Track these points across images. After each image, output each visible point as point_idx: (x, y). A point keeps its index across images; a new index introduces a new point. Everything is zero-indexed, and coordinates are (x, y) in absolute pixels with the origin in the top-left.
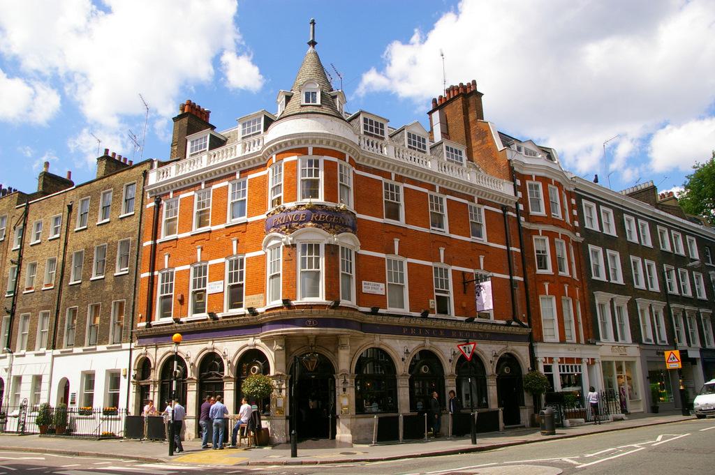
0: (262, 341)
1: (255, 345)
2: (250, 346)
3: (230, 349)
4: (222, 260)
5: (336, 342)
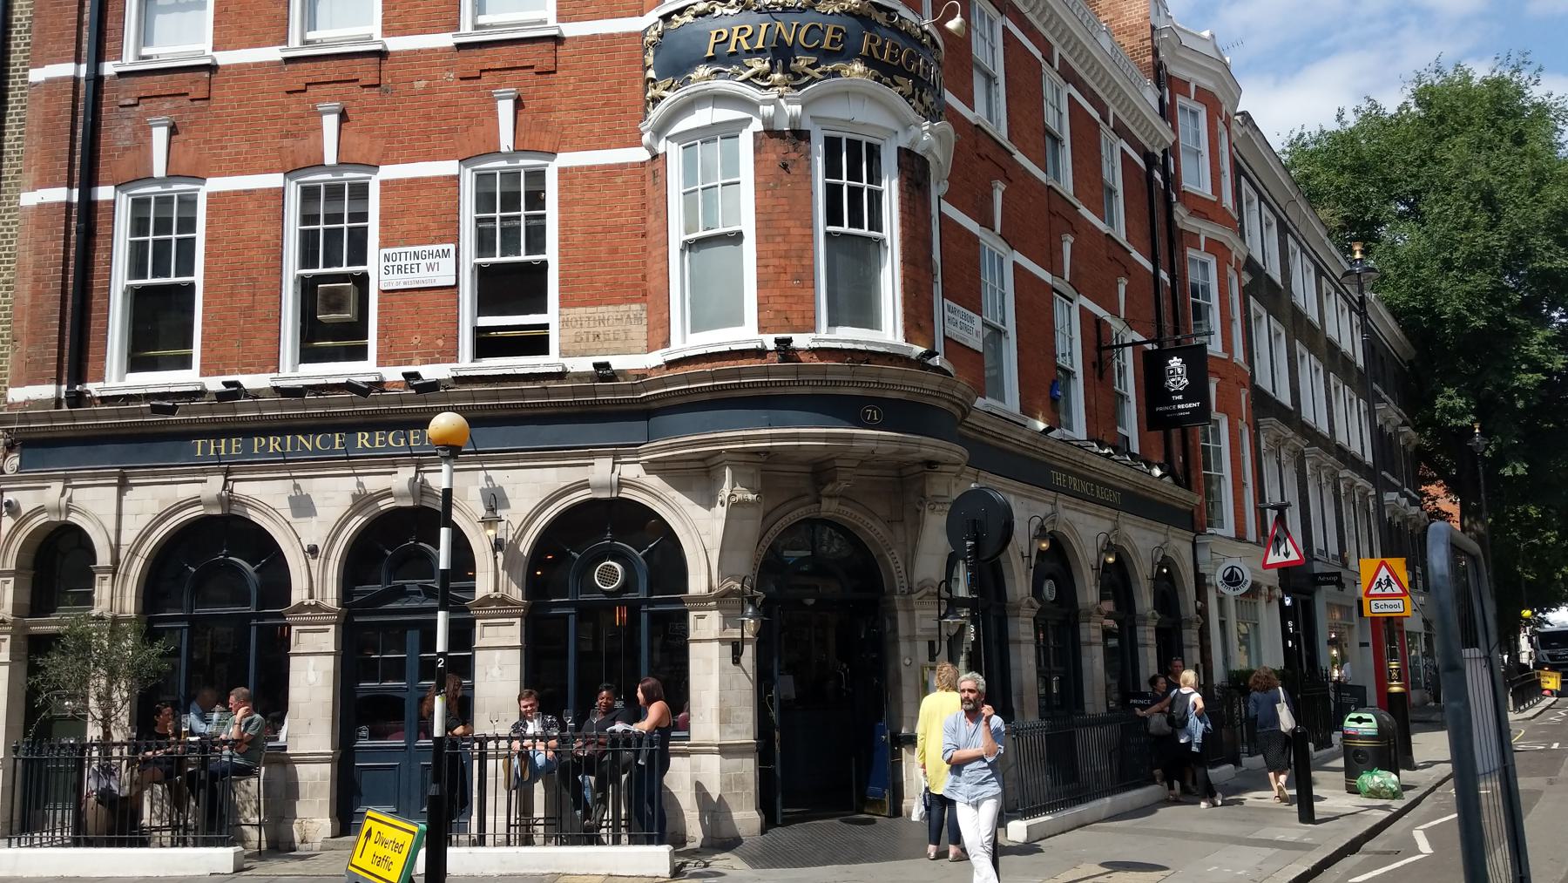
0: (648, 471)
1: (621, 484)
2: (207, 504)
3: (506, 503)
4: (449, 167)
5: (903, 485)
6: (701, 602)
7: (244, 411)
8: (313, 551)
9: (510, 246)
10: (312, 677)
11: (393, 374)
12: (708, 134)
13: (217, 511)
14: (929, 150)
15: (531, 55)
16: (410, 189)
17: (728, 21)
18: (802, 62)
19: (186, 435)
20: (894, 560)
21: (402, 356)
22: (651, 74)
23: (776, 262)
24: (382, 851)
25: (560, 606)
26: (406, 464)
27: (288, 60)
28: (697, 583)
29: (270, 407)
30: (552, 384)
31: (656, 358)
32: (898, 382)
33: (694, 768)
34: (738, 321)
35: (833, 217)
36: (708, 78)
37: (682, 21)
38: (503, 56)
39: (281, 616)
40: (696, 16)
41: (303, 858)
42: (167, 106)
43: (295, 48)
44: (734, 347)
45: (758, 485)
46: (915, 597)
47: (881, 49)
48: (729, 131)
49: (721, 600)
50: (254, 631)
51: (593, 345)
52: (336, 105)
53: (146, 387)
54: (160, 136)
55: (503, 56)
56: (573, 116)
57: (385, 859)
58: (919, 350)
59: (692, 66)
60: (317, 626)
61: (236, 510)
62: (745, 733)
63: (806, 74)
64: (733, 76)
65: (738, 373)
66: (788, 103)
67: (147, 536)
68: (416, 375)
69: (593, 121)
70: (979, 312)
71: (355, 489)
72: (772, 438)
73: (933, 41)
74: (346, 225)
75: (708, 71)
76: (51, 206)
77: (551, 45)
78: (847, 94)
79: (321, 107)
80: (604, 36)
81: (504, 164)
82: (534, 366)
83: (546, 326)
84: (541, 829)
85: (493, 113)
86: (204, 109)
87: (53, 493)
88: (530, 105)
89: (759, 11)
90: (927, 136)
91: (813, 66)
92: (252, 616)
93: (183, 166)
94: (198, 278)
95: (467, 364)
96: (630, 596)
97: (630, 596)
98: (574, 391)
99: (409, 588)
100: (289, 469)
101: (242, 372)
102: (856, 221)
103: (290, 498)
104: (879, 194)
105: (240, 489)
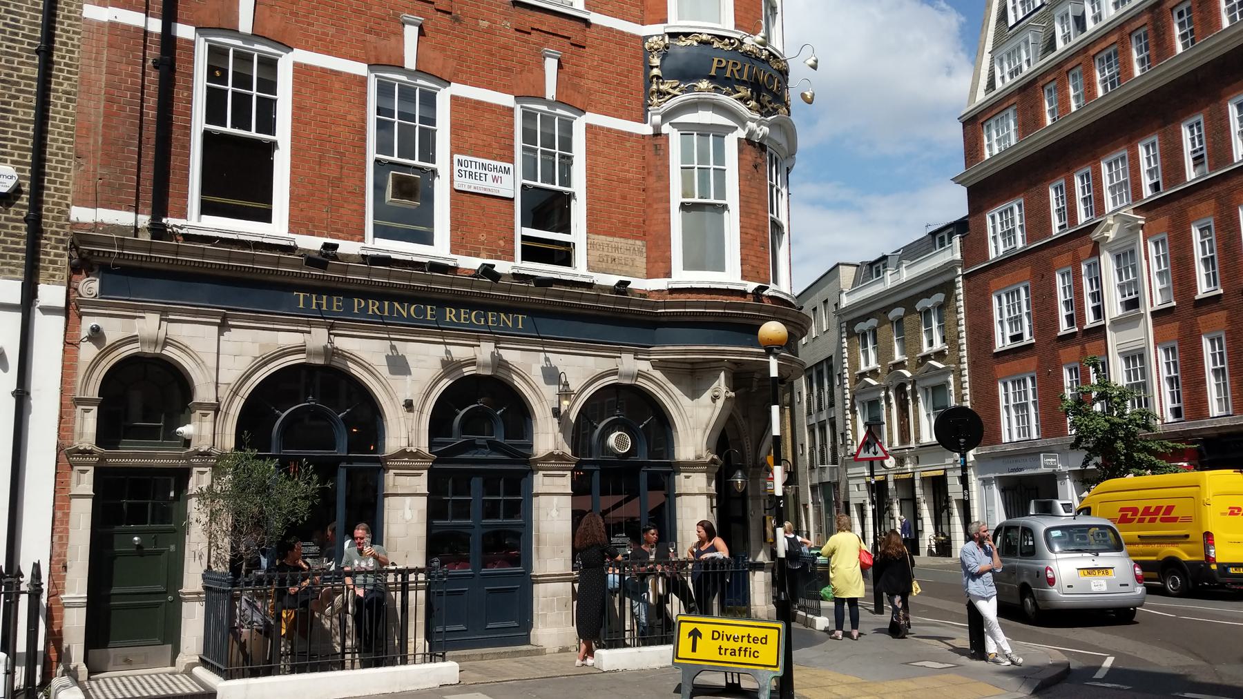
6: (691, 466)
7: (355, 273)
8: (409, 405)
12: (703, 130)
21: (472, 248)
26: (488, 340)
34: (720, 266)
38: (549, 23)
51: (611, 266)
53: (239, 233)
55: (549, 23)
56: (597, 86)
60: (412, 471)
61: (337, 362)
64: (728, 94)
65: (253, 259)
69: (610, 94)
76: (126, 28)
79: (406, 16)
87: (148, 325)
88: (566, 66)
92: (643, 464)
97: (632, 459)
98: (598, 298)
100: (388, 332)
103: (387, 357)
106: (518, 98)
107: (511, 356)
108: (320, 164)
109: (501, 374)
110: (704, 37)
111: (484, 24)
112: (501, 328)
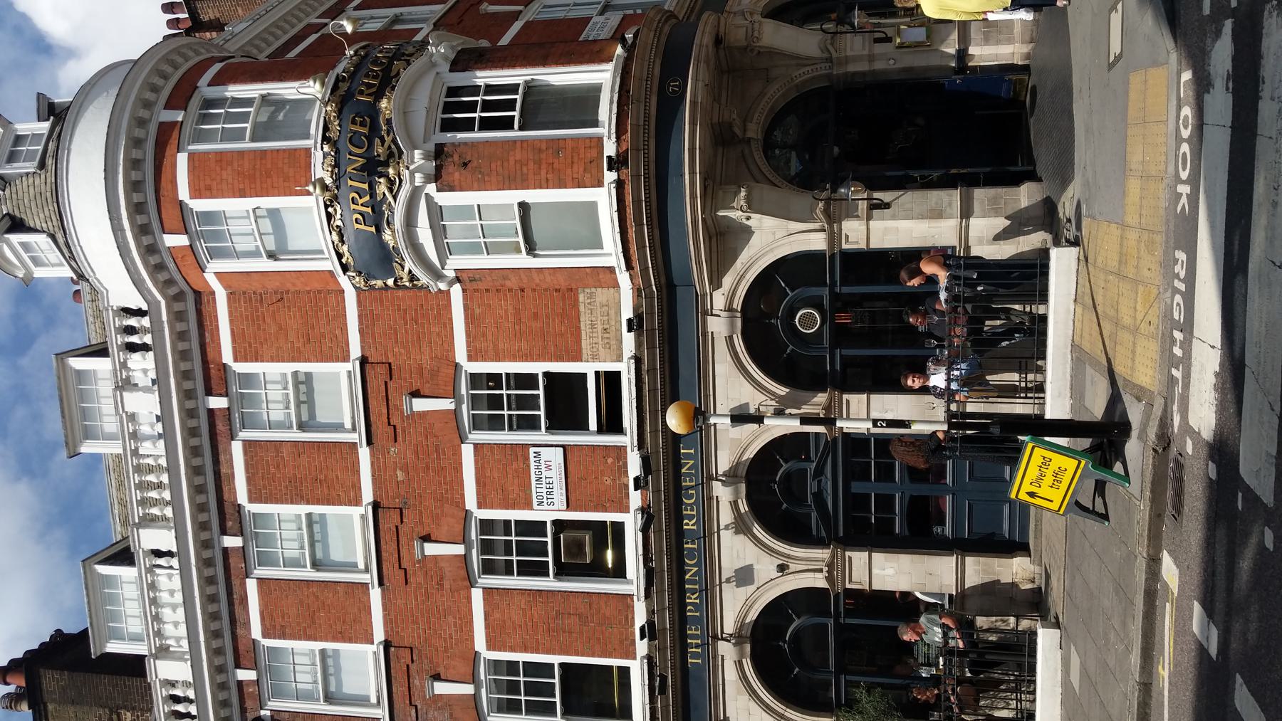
0: (719, 286)
1: (730, 309)
2: (742, 655)
3: (743, 408)
4: (467, 452)
5: (737, 66)
6: (833, 238)
8: (782, 568)
9: (531, 402)
10: (889, 572)
11: (635, 499)
12: (439, 232)
13: (748, 648)
14: (452, 48)
15: (376, 384)
16: (485, 485)
17: (346, 214)
18: (379, 150)
19: (684, 672)
20: (801, 75)
22: (390, 282)
23: (543, 172)
24: (1049, 479)
25: (832, 361)
26: (710, 489)
27: (381, 584)
28: (817, 242)
29: (661, 601)
30: (645, 367)
31: (624, 279)
32: (646, 64)
33: (980, 242)
34: (593, 206)
35: (506, 124)
36: (393, 232)
37: (347, 254)
38: (377, 406)
39: (837, 596)
40: (343, 242)
41: (1048, 577)
42: (417, 682)
43: (371, 578)
44: (615, 208)
45: (733, 188)
46: (834, 55)
47: (369, 86)
48: (436, 213)
49: (833, 218)
50: (849, 621)
51: (612, 335)
52: (416, 544)
53: (644, 704)
54: (441, 688)
55: (377, 406)
57: (1055, 475)
58: (619, 50)
59: (383, 245)
60: (847, 566)
61: (747, 632)
62: (953, 197)
63: (390, 147)
65: (637, 202)
66: (413, 162)
67: (767, 706)
68: (637, 480)
69: (430, 333)
70: (588, 20)
71: (730, 532)
72: (692, 172)
73: (363, 48)
74: (513, 538)
75: (388, 231)
77: (368, 366)
78: (405, 113)
79: (418, 556)
80: (361, 322)
81: (464, 407)
82: (630, 382)
83: (597, 373)
84: (1031, 377)
85: (423, 415)
86: (420, 651)
88: (416, 385)
89: (338, 188)
90: (440, 50)
91: (383, 141)
92: (832, 292)
93: (466, 669)
94: (555, 659)
95: (628, 439)
96: (826, 302)
97: (826, 302)
98: (651, 347)
99: (815, 489)
100: (713, 586)
101: (633, 625)
102: (510, 105)
103: (737, 586)
104: (487, 86)
105: (729, 627)
106: (463, 441)
107: (724, 462)
108: (570, 632)
109: (743, 471)
110: (335, 237)
111: (400, 475)
112: (697, 471)
